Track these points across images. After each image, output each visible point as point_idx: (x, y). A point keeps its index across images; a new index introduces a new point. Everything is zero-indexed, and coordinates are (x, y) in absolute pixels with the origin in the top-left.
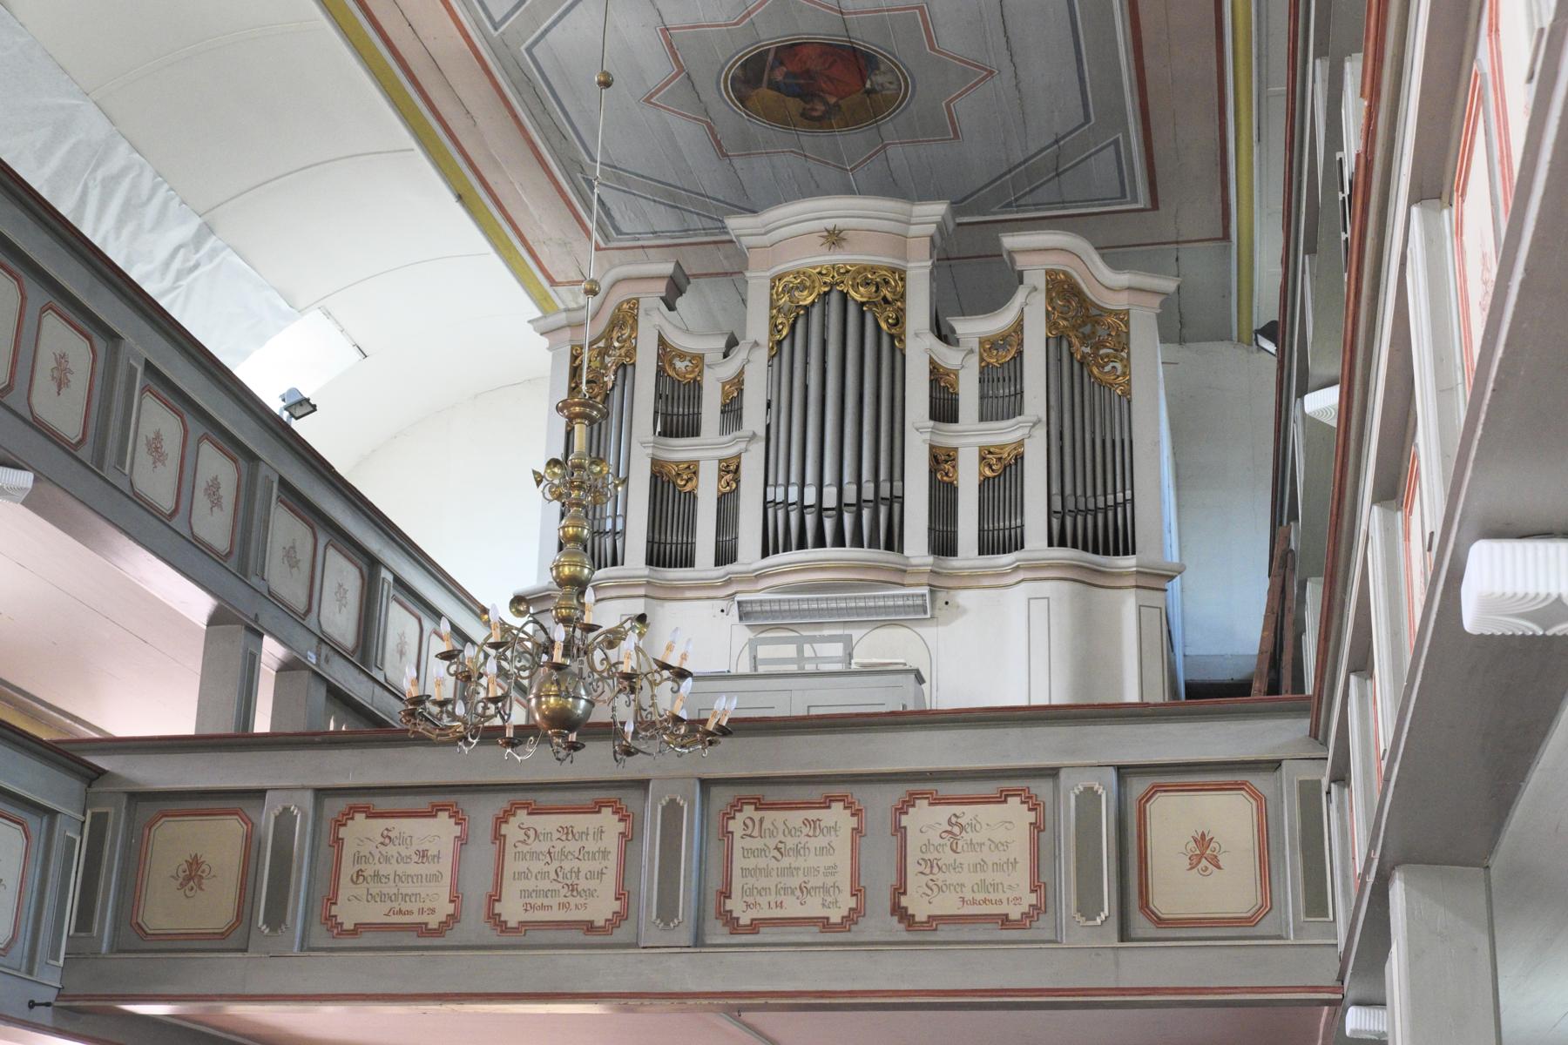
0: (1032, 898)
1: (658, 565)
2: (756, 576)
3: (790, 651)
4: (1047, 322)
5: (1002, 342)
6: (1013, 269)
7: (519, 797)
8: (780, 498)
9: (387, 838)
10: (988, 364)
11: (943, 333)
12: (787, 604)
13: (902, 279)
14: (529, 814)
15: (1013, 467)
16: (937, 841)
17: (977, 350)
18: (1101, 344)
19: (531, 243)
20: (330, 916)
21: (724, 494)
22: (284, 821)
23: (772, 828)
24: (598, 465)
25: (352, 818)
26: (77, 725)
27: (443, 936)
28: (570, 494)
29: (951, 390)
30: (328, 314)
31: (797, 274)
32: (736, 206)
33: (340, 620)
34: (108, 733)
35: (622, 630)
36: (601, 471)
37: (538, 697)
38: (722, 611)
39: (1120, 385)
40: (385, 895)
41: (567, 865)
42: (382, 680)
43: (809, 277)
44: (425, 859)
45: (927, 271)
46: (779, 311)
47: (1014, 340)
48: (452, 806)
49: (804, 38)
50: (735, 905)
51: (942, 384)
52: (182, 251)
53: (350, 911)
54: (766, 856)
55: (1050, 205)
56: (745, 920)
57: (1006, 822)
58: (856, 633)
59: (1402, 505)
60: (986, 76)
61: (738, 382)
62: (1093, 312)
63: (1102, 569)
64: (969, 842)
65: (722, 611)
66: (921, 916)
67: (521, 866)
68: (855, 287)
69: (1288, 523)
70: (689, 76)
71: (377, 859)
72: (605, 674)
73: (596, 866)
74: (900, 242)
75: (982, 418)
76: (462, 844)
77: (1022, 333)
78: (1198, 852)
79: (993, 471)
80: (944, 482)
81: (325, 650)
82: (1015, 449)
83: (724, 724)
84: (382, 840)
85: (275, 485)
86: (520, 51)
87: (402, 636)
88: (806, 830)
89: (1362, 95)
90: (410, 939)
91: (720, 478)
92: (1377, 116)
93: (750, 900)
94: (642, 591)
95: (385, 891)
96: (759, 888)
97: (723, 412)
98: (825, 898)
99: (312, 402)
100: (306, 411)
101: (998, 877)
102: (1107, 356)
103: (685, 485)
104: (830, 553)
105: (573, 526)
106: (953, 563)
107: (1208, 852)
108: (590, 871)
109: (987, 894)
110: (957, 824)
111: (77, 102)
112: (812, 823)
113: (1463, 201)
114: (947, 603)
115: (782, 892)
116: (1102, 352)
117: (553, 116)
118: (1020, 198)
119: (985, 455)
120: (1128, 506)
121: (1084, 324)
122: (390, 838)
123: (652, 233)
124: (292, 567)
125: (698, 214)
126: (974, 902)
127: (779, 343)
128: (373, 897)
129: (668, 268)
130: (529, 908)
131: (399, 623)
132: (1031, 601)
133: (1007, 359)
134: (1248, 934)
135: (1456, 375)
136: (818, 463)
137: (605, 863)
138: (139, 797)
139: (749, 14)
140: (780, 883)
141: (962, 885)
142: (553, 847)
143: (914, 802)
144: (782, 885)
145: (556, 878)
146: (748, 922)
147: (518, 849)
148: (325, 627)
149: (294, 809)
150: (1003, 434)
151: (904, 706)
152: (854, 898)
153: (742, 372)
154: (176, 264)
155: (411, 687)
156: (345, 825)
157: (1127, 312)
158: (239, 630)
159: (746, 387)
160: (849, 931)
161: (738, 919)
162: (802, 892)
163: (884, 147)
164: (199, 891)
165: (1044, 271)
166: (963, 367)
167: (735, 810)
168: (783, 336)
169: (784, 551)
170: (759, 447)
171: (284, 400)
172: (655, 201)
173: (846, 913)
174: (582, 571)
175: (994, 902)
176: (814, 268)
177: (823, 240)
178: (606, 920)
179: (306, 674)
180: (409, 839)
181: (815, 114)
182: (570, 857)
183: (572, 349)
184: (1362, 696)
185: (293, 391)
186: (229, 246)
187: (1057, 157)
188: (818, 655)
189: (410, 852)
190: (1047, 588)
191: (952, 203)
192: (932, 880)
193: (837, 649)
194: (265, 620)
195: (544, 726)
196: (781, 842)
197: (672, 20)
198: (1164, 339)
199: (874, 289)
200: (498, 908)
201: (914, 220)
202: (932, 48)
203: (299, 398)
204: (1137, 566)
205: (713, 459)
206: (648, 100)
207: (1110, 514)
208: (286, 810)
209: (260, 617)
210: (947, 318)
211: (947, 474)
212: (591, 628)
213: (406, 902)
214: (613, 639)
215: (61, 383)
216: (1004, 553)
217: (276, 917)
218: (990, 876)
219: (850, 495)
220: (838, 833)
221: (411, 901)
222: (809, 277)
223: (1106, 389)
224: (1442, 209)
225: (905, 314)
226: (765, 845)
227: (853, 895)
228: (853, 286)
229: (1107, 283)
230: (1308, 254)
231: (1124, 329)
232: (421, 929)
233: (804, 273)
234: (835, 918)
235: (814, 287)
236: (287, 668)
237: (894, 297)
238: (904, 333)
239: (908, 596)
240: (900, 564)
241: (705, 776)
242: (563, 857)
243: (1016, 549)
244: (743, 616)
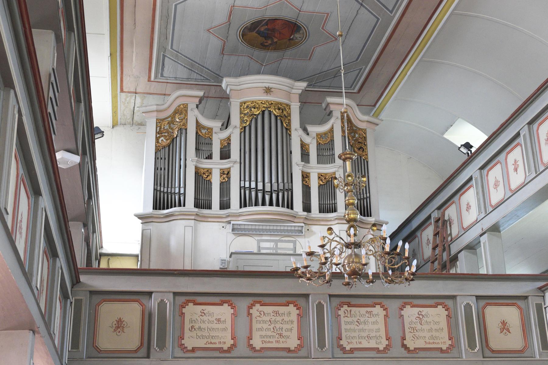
0: (450, 342)
2: (239, 215)
3: (271, 245)
4: (342, 131)
5: (324, 136)
7: (188, 298)
9: (203, 313)
11: (305, 130)
12: (287, 227)
14: (261, 305)
15: (330, 182)
16: (414, 320)
17: (316, 138)
20: (182, 344)
21: (222, 182)
22: (162, 305)
23: (355, 314)
25: (188, 305)
27: (231, 353)
38: (223, 227)
40: (204, 336)
41: (278, 326)
43: (258, 104)
44: (220, 322)
48: (230, 301)
50: (343, 342)
51: (304, 149)
53: (189, 342)
54: (353, 325)
56: (348, 348)
57: (438, 314)
60: (334, 40)
62: (354, 128)
64: (426, 321)
66: (412, 348)
67: (259, 326)
68: (275, 109)
71: (199, 322)
73: (289, 326)
76: (235, 317)
78: (503, 327)
79: (323, 182)
82: (331, 175)
84: (201, 314)
88: (367, 315)
90: (217, 354)
91: (221, 176)
93: (349, 341)
94: (193, 217)
95: (204, 334)
96: (264, 335)
98: (377, 341)
100: (99, 137)
101: (437, 334)
103: (207, 178)
104: (267, 208)
105: (352, 200)
107: (506, 327)
108: (287, 329)
109: (434, 340)
110: (421, 314)
112: (369, 312)
114: (308, 230)
115: (361, 338)
117: (168, 30)
119: (320, 176)
122: (204, 313)
123: (175, 78)
126: (429, 343)
127: (245, 127)
128: (199, 337)
129: (201, 94)
130: (264, 342)
132: (340, 231)
134: (277, 355)
136: (262, 174)
137: (292, 325)
138: (93, 293)
140: (360, 335)
141: (425, 337)
142: (271, 319)
143: (288, 305)
144: (360, 335)
145: (273, 331)
146: (349, 349)
147: (257, 319)
149: (323, 302)
152: (387, 341)
156: (185, 307)
157: (365, 130)
160: (387, 353)
161: (345, 348)
162: (368, 338)
164: (123, 333)
167: (341, 307)
168: (247, 125)
169: (249, 206)
173: (385, 346)
174: (357, 216)
175: (436, 343)
176: (260, 101)
178: (295, 348)
180: (212, 314)
182: (278, 323)
189: (214, 319)
192: (414, 335)
193: (291, 245)
196: (358, 319)
199: (281, 111)
200: (251, 342)
201: (294, 87)
204: (374, 221)
205: (218, 168)
206: (208, 30)
208: (162, 300)
210: (306, 125)
211: (306, 182)
213: (213, 339)
217: (162, 345)
218: (434, 334)
219: (275, 187)
220: (379, 317)
221: (215, 339)
222: (258, 104)
226: (353, 320)
227: (387, 340)
228: (274, 109)
232: (220, 350)
233: (255, 102)
234: (381, 348)
235: (260, 108)
237: (288, 115)
238: (290, 128)
240: (295, 214)
241: (331, 294)
242: (276, 323)
244: (233, 230)
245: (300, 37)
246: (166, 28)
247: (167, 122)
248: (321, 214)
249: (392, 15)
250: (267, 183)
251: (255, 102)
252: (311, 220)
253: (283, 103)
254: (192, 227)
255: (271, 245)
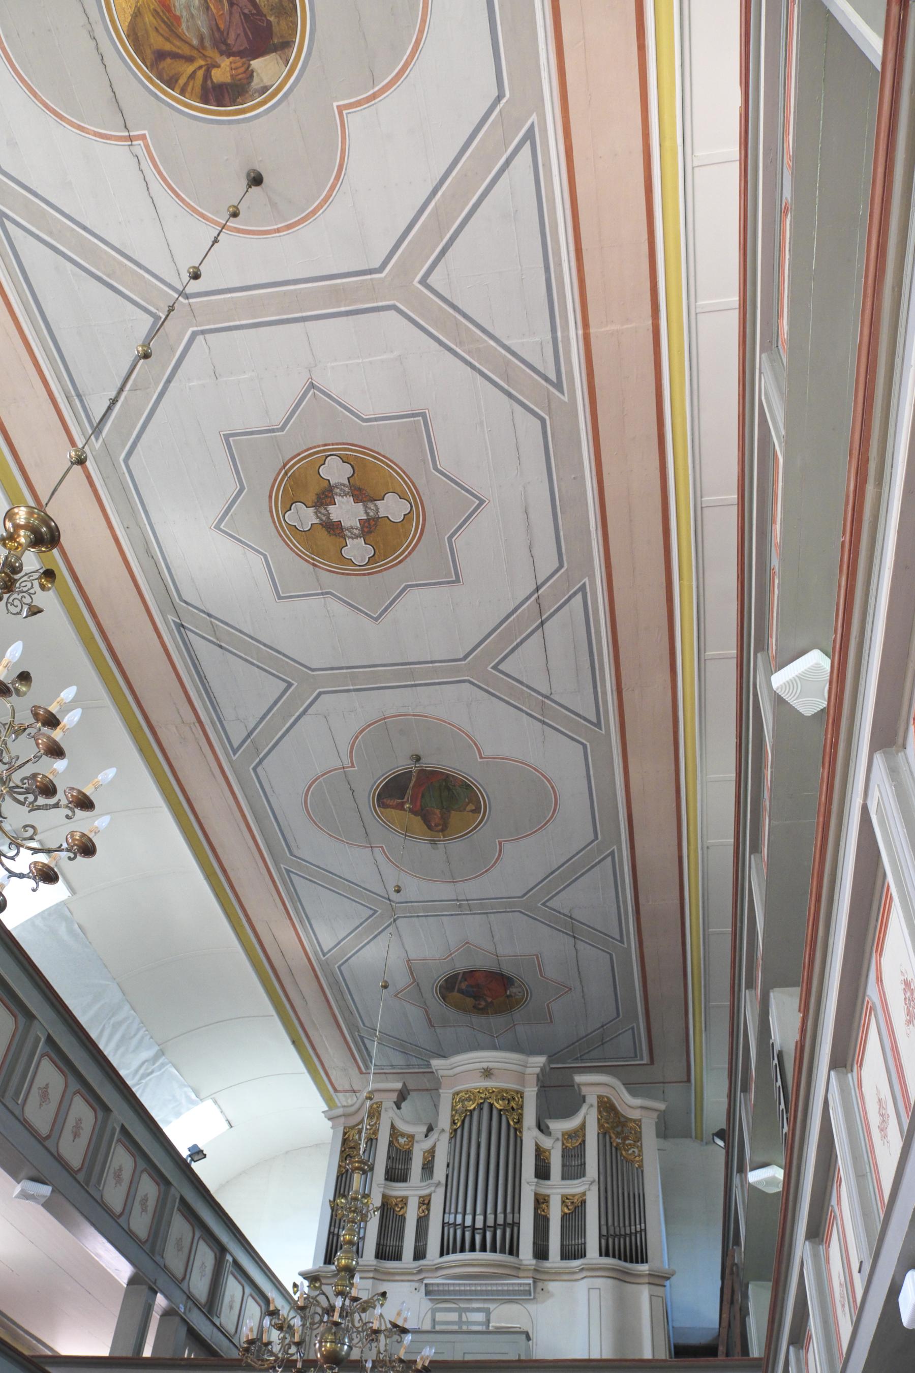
1: (381, 1259)
3: (454, 1317)
6: (580, 1094)
8: (452, 1221)
10: (567, 1147)
11: (541, 1127)
13: (522, 1097)
15: (580, 1207)
18: (625, 1138)
19: (327, 1068)
24: (366, 1198)
26: (39, 1345)
28: (349, 1215)
29: (546, 1161)
30: (216, 1102)
31: (467, 1092)
32: (435, 1053)
33: (199, 1286)
34: (57, 1352)
35: (372, 1301)
36: (368, 1202)
37: (320, 1342)
39: (637, 1162)
42: (218, 1324)
43: (473, 1094)
45: (535, 1093)
46: (456, 1113)
47: (580, 1134)
49: (478, 968)
52: (146, 1063)
55: (599, 1060)
58: (492, 1306)
59: (822, 1241)
60: (568, 991)
61: (432, 1152)
62: (622, 1119)
63: (629, 1271)
65: (416, 1289)
68: (497, 1101)
69: (733, 1247)
70: (418, 984)
72: (360, 1329)
74: (521, 1077)
75: (563, 1178)
77: (585, 1129)
79: (569, 1209)
80: (542, 1215)
81: (190, 1303)
82: (581, 1197)
83: (426, 1365)
85: (178, 1200)
86: (334, 967)
87: (232, 1296)
89: (799, 1011)
91: (419, 1207)
92: (807, 1021)
94: (371, 1275)
97: (423, 1168)
99: (205, 1152)
100: (199, 1158)
102: (630, 1144)
103: (399, 1211)
104: (478, 1255)
106: (547, 1264)
111: (107, 983)
113: (861, 1069)
114: (542, 1289)
116: (627, 1142)
118: (583, 1055)
119: (565, 1200)
120: (643, 1234)
121: (617, 1126)
124: (179, 1250)
125: (415, 1057)
127: (456, 1130)
129: (399, 1085)
131: (233, 1288)
133: (577, 1144)
135: (865, 1168)
139: (451, 954)
148: (191, 1289)
150: (575, 1188)
151: (519, 1355)
153: (434, 1146)
154: (141, 1071)
155: (249, 1333)
157: (640, 1120)
158: (144, 1288)
159: (436, 1154)
163: (514, 1025)
165: (596, 1097)
166: (553, 1148)
169: (453, 1253)
170: (442, 1189)
171: (189, 1151)
172: (394, 1049)
174: (352, 1263)
177: (482, 1074)
179: (177, 1319)
181: (480, 1007)
183: (344, 1128)
184: (798, 1360)
185: (195, 1146)
186: (171, 1062)
187: (603, 1035)
188: (469, 1320)
190: (599, 1282)
191: (549, 1056)
193: (480, 1317)
194: (160, 1283)
195: (322, 1361)
197: (412, 956)
198: (658, 1136)
199: (507, 1102)
201: (528, 1065)
202: (541, 975)
203: (198, 1150)
204: (649, 1270)
206: (396, 996)
207: (633, 1238)
209: (157, 1282)
211: (543, 1211)
212: (355, 1299)
214: (366, 1306)
215: (76, 1135)
216: (575, 1259)
219: (490, 1222)
222: (473, 1094)
223: (630, 1165)
224: (847, 1073)
225: (522, 1117)
229: (626, 1101)
230: (743, 1092)
231: (639, 1130)
233: (470, 1092)
235: (475, 1100)
236: (168, 1314)
238: (522, 1127)
239: (520, 1284)
243: (581, 1257)
244: (428, 1293)
245: (519, 992)
246: (344, 999)
247: (356, 1131)
248: (565, 1261)
249: (626, 946)
250: (490, 1214)
251: (470, 1092)
252: (548, 1273)
253: (511, 1090)
254: (369, 1290)
255: (454, 1317)
